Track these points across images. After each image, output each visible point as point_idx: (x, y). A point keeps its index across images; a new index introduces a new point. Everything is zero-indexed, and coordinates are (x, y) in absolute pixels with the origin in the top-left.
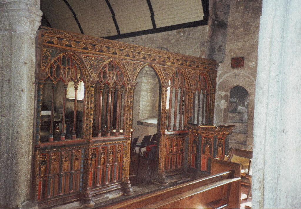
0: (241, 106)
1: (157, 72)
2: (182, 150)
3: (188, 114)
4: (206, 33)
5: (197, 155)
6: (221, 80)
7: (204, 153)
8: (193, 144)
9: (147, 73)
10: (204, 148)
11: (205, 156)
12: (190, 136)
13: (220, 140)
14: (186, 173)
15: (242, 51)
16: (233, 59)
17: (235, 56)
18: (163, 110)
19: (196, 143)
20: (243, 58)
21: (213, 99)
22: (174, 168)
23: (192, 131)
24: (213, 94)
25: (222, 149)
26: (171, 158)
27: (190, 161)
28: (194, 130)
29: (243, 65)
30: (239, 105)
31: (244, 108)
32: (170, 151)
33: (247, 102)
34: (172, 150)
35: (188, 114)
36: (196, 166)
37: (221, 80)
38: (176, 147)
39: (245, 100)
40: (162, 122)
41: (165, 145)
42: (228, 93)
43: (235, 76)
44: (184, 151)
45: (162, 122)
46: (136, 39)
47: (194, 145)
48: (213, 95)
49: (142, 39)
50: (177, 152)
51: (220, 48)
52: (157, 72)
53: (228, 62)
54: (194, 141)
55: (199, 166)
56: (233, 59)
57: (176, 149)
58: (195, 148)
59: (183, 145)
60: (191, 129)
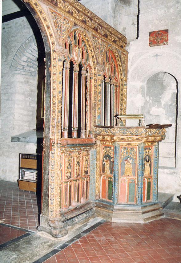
0: (156, 106)
1: (43, 20)
2: (87, 172)
3: (95, 112)
4: (108, 3)
5: (111, 178)
6: (135, 66)
7: (123, 173)
8: (103, 161)
9: (25, 69)
10: (123, 165)
11: (125, 178)
12: (99, 148)
13: (147, 151)
14: (94, 209)
15: (163, 22)
16: (151, 34)
17: (154, 30)
18: (54, 97)
19: (110, 157)
20: (166, 31)
21: (125, 93)
22: (74, 204)
23: (103, 138)
24: (125, 85)
25: (150, 165)
26: (70, 187)
27: (99, 188)
28: (106, 137)
29: (167, 41)
30: (153, 106)
31: (161, 109)
32: (69, 174)
33: (165, 101)
34: (71, 173)
35: (95, 112)
36: (110, 197)
37: (135, 66)
38: (77, 168)
39: (161, 98)
40: (53, 119)
41: (59, 163)
42: (145, 84)
43: (156, 57)
44: (90, 173)
45: (53, 119)
46: (8, 25)
47: (106, 161)
48: (125, 87)
49: (16, 23)
50: (79, 175)
51: (124, 31)
52: (43, 20)
53: (145, 37)
54: (107, 156)
55: (116, 196)
56: (151, 34)
57: (78, 171)
58: (107, 167)
59: (88, 164)
60: (100, 135)
